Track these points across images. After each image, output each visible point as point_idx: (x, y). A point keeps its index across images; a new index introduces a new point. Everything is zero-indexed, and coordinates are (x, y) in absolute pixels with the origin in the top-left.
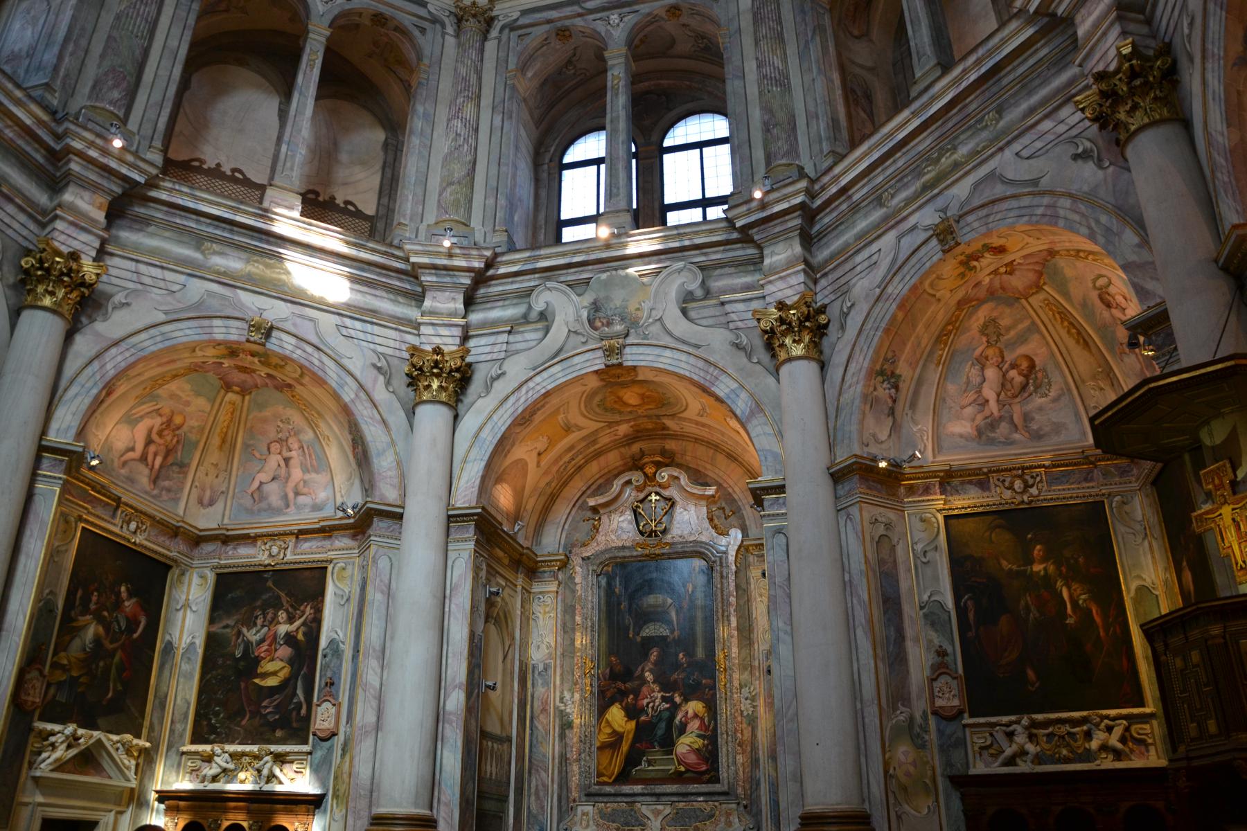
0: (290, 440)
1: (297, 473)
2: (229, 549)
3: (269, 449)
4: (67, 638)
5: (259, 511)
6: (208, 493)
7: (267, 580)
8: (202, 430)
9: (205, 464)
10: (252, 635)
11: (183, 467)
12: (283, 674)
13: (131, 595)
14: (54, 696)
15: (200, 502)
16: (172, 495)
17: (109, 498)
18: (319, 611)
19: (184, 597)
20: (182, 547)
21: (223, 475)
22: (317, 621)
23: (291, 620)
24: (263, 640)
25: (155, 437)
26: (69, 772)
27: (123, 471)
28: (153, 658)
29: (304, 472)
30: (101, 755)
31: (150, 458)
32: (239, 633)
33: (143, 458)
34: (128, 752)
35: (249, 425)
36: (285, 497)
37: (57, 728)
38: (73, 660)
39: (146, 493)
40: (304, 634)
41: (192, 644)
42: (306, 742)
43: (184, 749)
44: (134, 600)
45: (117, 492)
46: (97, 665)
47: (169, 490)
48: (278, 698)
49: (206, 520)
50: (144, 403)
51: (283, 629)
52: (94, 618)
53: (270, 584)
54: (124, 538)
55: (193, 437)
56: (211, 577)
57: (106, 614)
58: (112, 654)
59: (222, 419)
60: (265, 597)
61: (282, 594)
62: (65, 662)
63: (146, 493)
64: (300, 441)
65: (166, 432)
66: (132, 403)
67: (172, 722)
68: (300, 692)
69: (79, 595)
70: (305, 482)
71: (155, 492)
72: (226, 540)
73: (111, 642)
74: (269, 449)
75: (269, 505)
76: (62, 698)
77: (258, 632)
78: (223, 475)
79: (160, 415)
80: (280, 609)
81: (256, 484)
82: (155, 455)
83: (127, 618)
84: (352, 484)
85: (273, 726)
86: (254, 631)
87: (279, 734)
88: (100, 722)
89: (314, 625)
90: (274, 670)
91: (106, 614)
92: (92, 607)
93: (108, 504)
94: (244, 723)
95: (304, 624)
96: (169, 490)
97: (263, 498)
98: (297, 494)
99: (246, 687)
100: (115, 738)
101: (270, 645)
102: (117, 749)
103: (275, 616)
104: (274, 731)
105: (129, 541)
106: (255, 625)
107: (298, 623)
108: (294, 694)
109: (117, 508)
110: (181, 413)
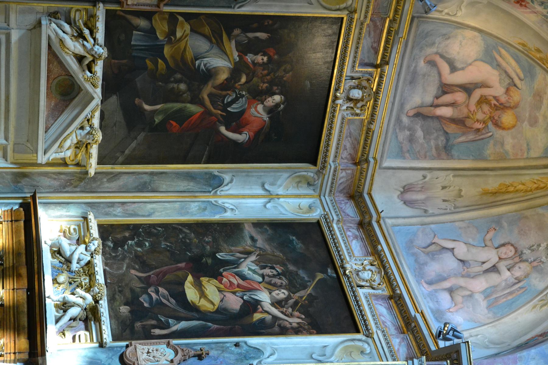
0: (523, 265)
1: (480, 285)
2: (353, 232)
3: (503, 245)
4: (207, 30)
5: (414, 254)
6: (420, 196)
7: (325, 272)
8: (503, 157)
9: (458, 180)
10: (248, 267)
11: (446, 150)
12: (204, 305)
13: (271, 111)
14: (137, 28)
15: (406, 189)
16: (406, 146)
17: (385, 49)
18: (297, 331)
19: (281, 191)
20: (342, 176)
21: (449, 206)
22: (284, 331)
23: (277, 304)
24: (243, 278)
25: (477, 94)
26: (49, 71)
27: (422, 64)
28: (200, 163)
29: (483, 292)
30: (75, 107)
31: (447, 98)
32: (248, 253)
33: (445, 89)
34: (78, 146)
35: (528, 213)
36: (441, 279)
37: (100, 36)
38: (182, 44)
39: (402, 106)
40: (262, 321)
41: (225, 210)
42: (115, 338)
43: (91, 216)
44: (266, 117)
45: (395, 58)
46: (179, 81)
47: (411, 139)
48: (172, 303)
49: (384, 197)
50: (518, 61)
51: (264, 297)
52: (236, 63)
53: (320, 276)
54: (339, 82)
55: (490, 150)
56: (315, 215)
57: (244, 79)
58: (196, 100)
59: (526, 179)
60: (302, 273)
61: (309, 290)
62: (179, 34)
63: (402, 106)
64: (527, 276)
65: (486, 108)
66: (514, 41)
67: (123, 203)
68: (183, 325)
69: (258, 34)
70: (471, 296)
71: (405, 120)
72: (365, 227)
73: (210, 95)
74: (503, 245)
75: (426, 264)
76: (137, 38)
77: (254, 272)
78: (449, 206)
79: (508, 90)
80: (289, 290)
81: (450, 245)
82: (453, 105)
83: (242, 113)
84: (487, 347)
85: (133, 302)
86: (254, 267)
87: (124, 310)
88: (114, 99)
89: (276, 329)
90: (208, 295)
91: (244, 79)
92: (249, 58)
93: (377, 52)
94: (133, 272)
95: (275, 318)
96: (411, 139)
97: (433, 256)
98: (451, 291)
99: (180, 269)
100: (96, 122)
101: (239, 286)
102: (82, 128)
103: (280, 287)
104: (126, 304)
105: (337, 90)
106: (263, 268)
107: (275, 312)
108: (179, 319)
109: (376, 66)
110: (518, 118)
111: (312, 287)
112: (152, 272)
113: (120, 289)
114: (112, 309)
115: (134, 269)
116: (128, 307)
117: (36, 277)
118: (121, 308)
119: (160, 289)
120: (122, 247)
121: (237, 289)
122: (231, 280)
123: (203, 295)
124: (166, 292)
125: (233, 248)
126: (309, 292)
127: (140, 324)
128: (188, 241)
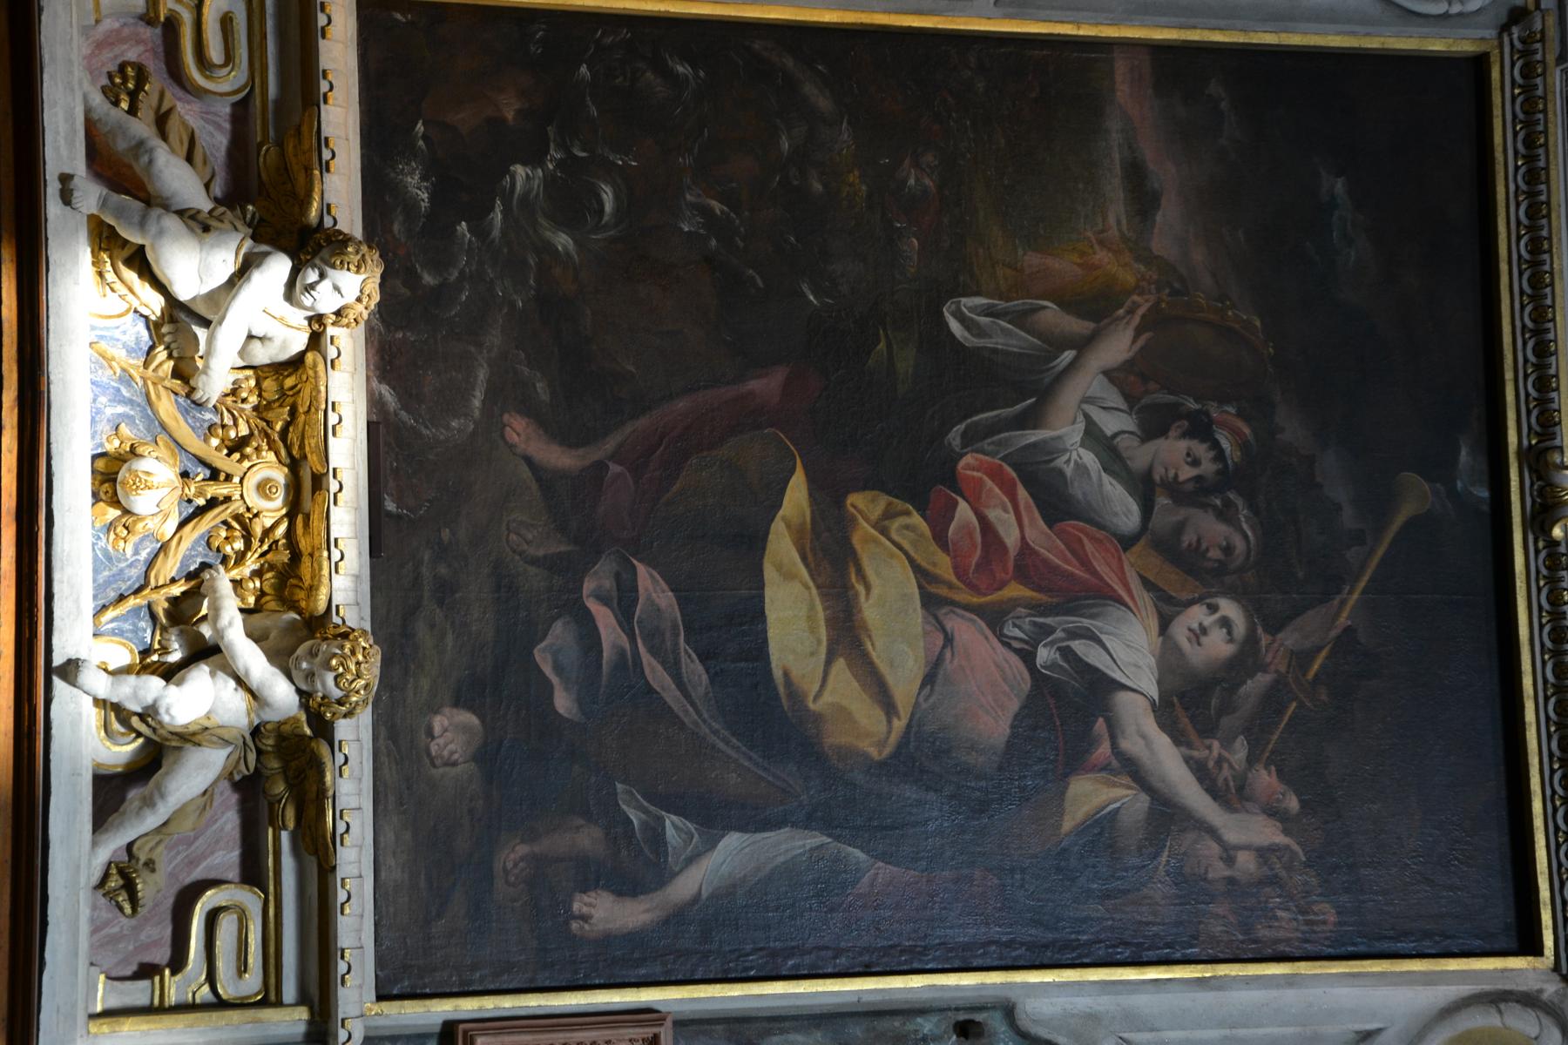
10: (1084, 420)
48: (681, 683)
53: (1415, 497)
95: (1167, 814)
101: (1028, 566)
104: (460, 701)
106: (1154, 425)
108: (715, 817)
111: (1362, 584)
112: (610, 444)
113: (443, 570)
114: (393, 735)
115: (528, 408)
116: (471, 719)
117: (1242, 1032)
118: (438, 723)
119: (645, 577)
120: (478, 217)
121: (1015, 590)
122: (993, 514)
123: (846, 634)
124: (666, 599)
125: (1032, 260)
126: (1343, 620)
127: (522, 849)
128: (817, 187)
